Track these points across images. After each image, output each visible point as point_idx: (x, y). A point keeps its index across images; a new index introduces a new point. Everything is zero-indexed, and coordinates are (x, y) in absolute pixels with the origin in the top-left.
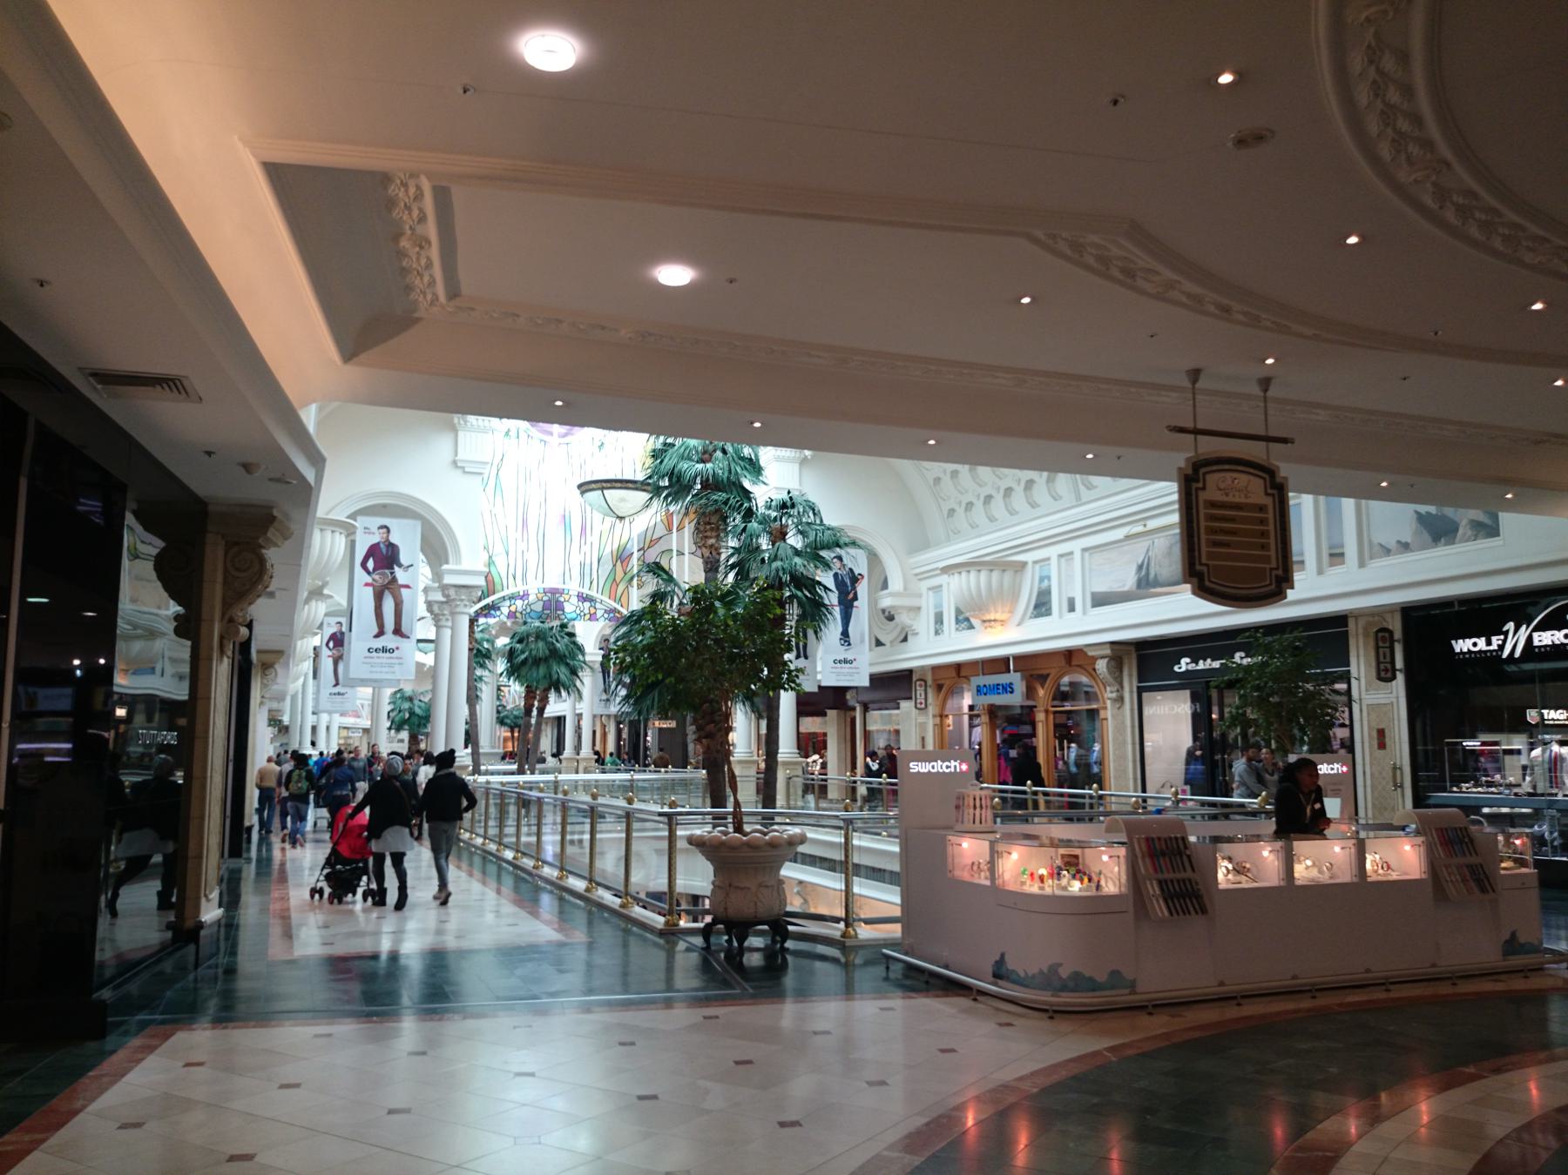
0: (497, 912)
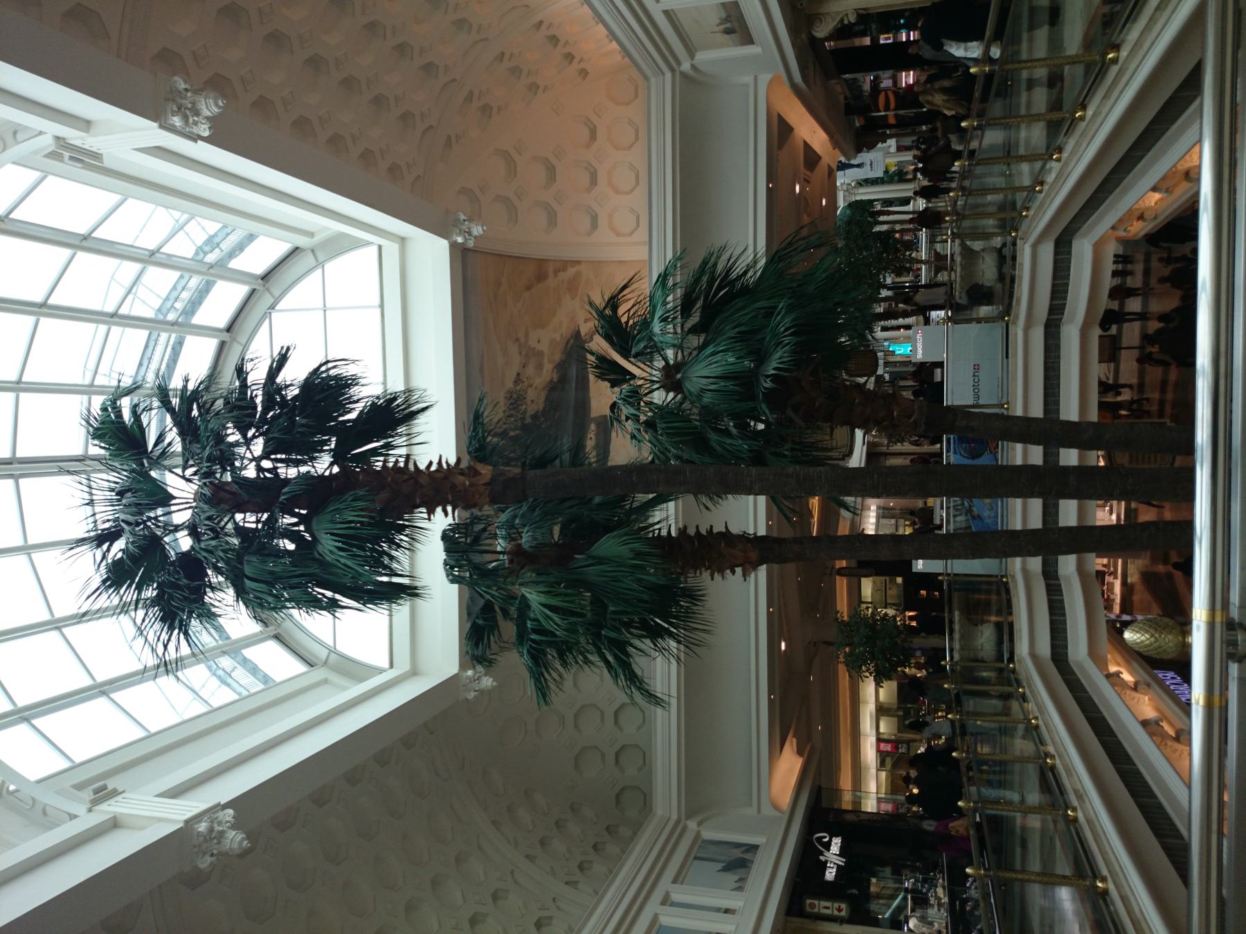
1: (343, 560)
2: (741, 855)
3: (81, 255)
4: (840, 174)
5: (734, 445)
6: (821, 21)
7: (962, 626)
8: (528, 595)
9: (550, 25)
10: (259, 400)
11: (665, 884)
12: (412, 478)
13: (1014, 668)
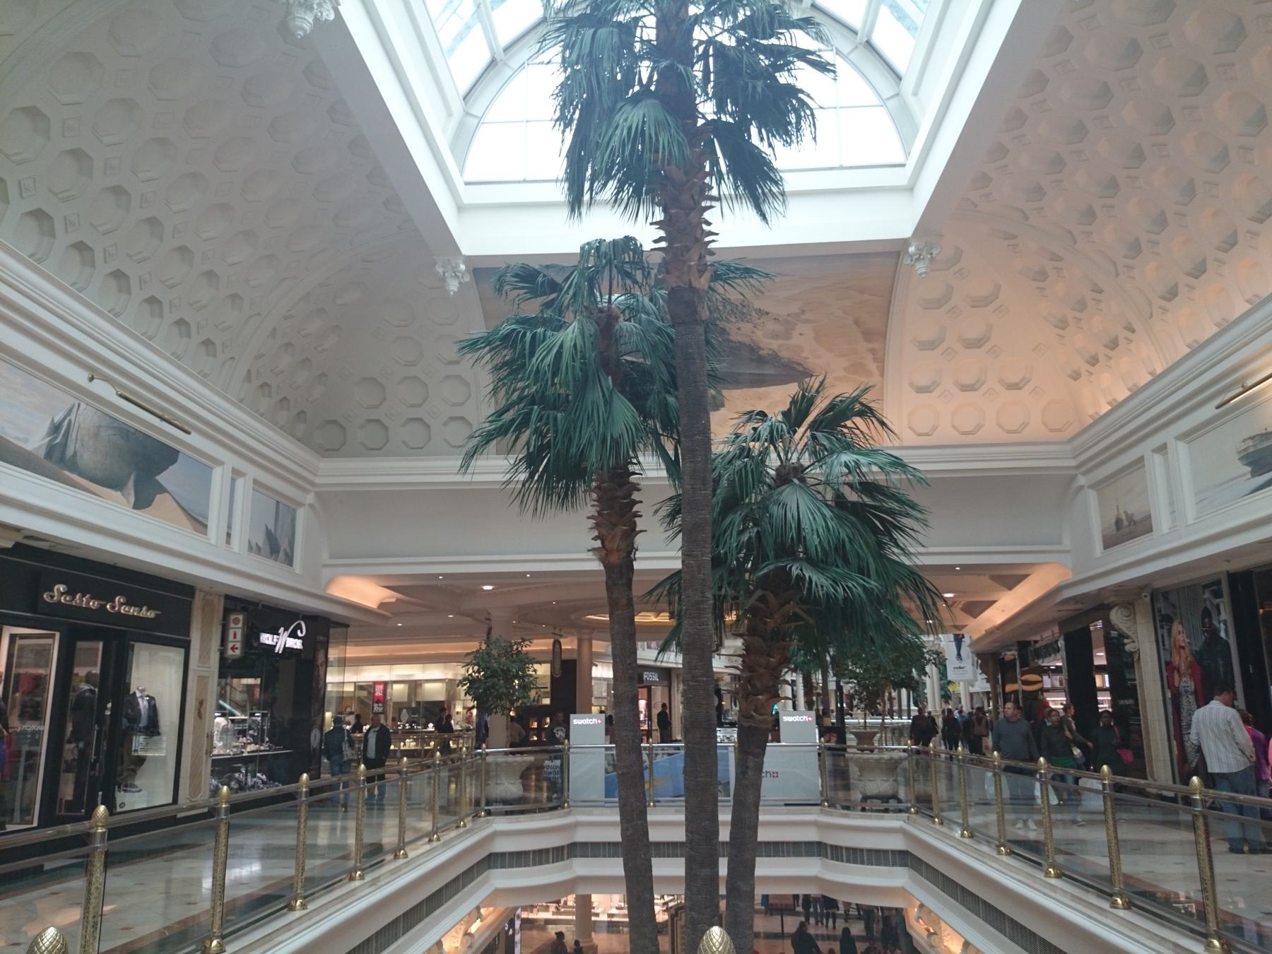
0: (168, 893)
1: (618, 132)
2: (282, 548)
4: (951, 637)
5: (731, 538)
6: (1128, 616)
7: (520, 763)
8: (571, 329)
9: (1130, 341)
10: (773, 41)
11: (252, 472)
12: (695, 203)
13: (480, 817)
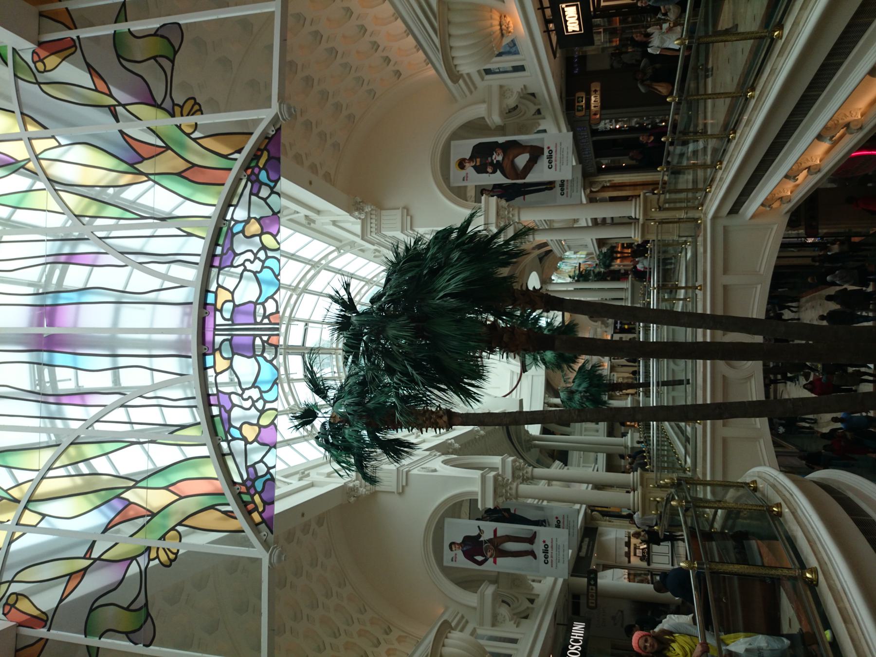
3: (290, 261)
